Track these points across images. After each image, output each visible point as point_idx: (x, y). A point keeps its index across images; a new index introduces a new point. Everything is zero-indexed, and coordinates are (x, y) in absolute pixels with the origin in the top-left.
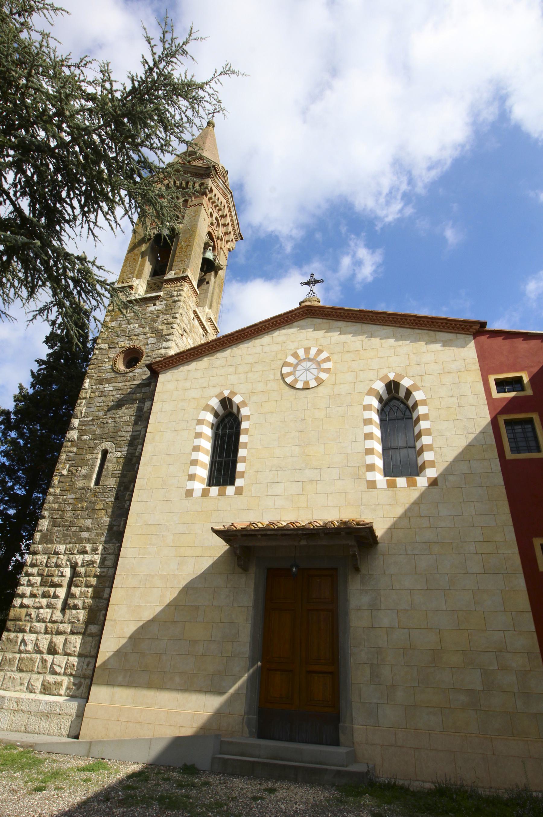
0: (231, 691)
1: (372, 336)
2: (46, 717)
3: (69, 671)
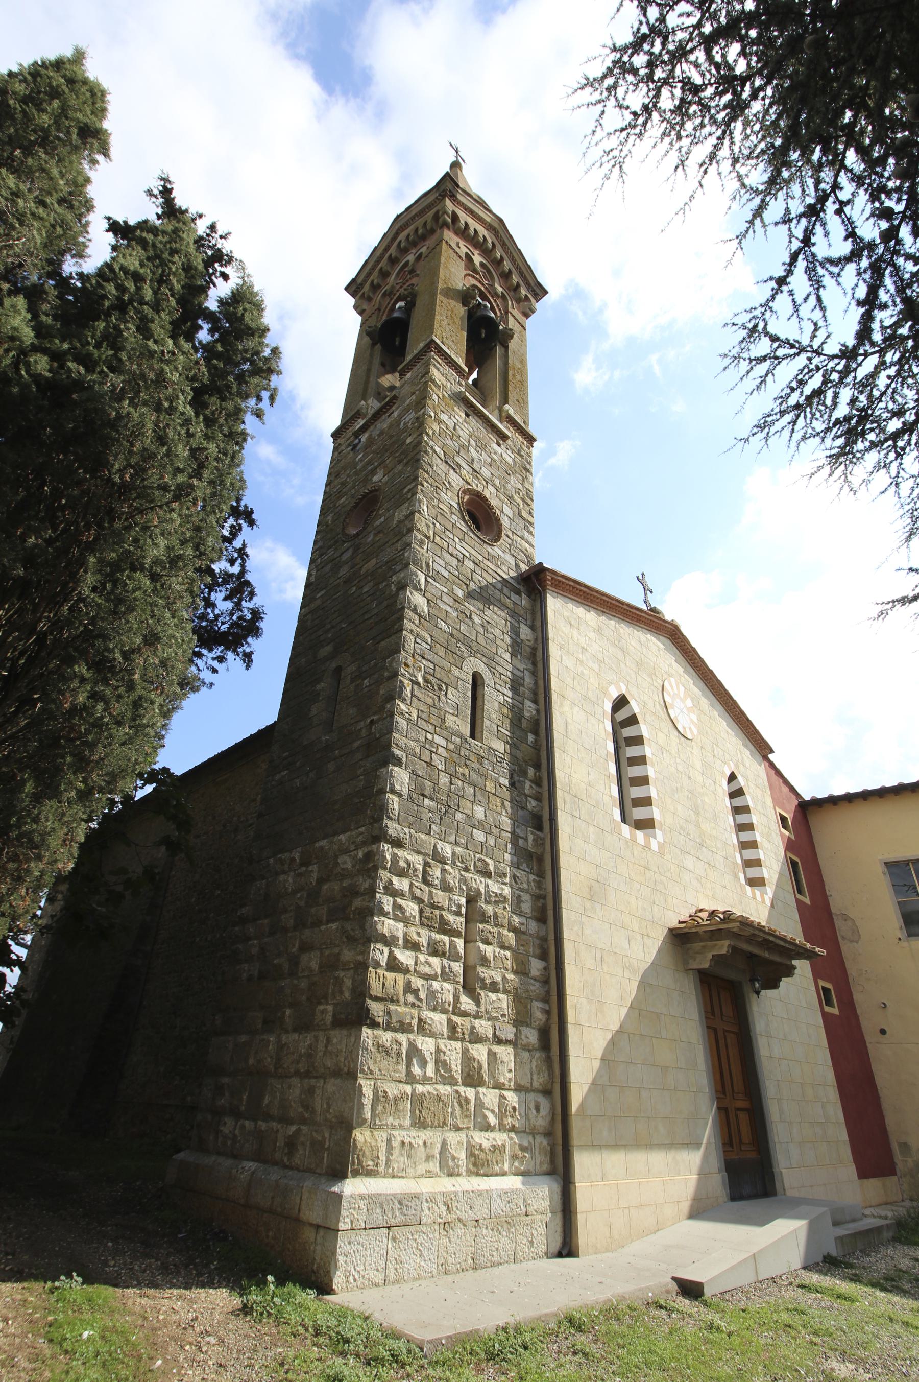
0: (705, 1141)
1: (746, 746)
2: (505, 1225)
3: (509, 1121)
